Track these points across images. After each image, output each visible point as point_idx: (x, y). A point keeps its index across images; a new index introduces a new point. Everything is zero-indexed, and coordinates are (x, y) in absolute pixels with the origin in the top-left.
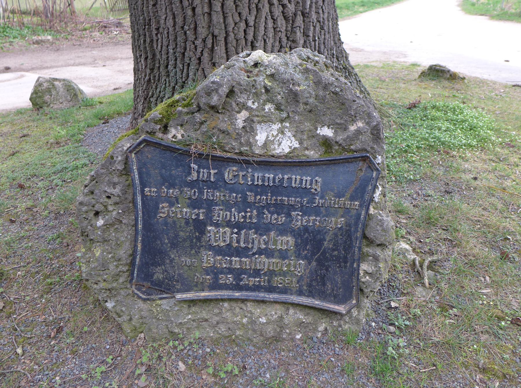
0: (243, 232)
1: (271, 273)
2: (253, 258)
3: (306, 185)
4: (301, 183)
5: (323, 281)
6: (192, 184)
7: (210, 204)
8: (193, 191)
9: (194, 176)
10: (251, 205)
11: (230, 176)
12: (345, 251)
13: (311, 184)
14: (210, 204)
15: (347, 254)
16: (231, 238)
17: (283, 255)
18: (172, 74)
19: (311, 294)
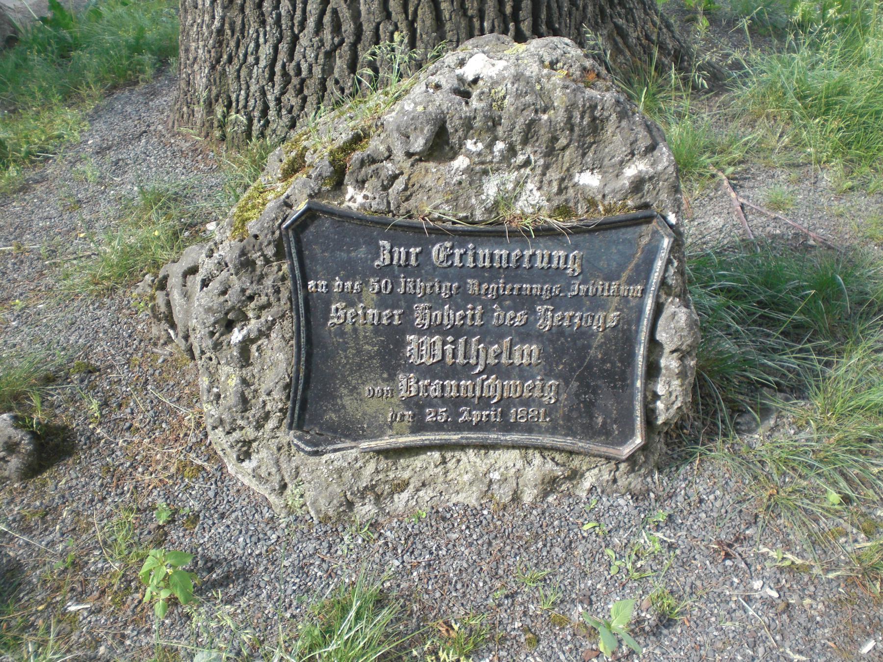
0: (461, 340)
1: (506, 403)
2: (479, 380)
3: (558, 263)
4: (550, 261)
5: (590, 406)
6: (382, 272)
7: (410, 299)
8: (384, 282)
9: (384, 258)
10: (475, 299)
11: (441, 256)
12: (623, 364)
13: (566, 263)
14: (410, 299)
15: (625, 366)
16: (444, 352)
17: (523, 373)
18: (270, 20)
19: (570, 432)
